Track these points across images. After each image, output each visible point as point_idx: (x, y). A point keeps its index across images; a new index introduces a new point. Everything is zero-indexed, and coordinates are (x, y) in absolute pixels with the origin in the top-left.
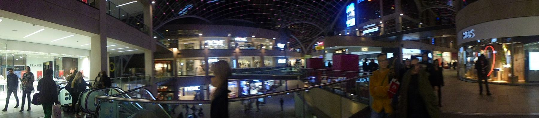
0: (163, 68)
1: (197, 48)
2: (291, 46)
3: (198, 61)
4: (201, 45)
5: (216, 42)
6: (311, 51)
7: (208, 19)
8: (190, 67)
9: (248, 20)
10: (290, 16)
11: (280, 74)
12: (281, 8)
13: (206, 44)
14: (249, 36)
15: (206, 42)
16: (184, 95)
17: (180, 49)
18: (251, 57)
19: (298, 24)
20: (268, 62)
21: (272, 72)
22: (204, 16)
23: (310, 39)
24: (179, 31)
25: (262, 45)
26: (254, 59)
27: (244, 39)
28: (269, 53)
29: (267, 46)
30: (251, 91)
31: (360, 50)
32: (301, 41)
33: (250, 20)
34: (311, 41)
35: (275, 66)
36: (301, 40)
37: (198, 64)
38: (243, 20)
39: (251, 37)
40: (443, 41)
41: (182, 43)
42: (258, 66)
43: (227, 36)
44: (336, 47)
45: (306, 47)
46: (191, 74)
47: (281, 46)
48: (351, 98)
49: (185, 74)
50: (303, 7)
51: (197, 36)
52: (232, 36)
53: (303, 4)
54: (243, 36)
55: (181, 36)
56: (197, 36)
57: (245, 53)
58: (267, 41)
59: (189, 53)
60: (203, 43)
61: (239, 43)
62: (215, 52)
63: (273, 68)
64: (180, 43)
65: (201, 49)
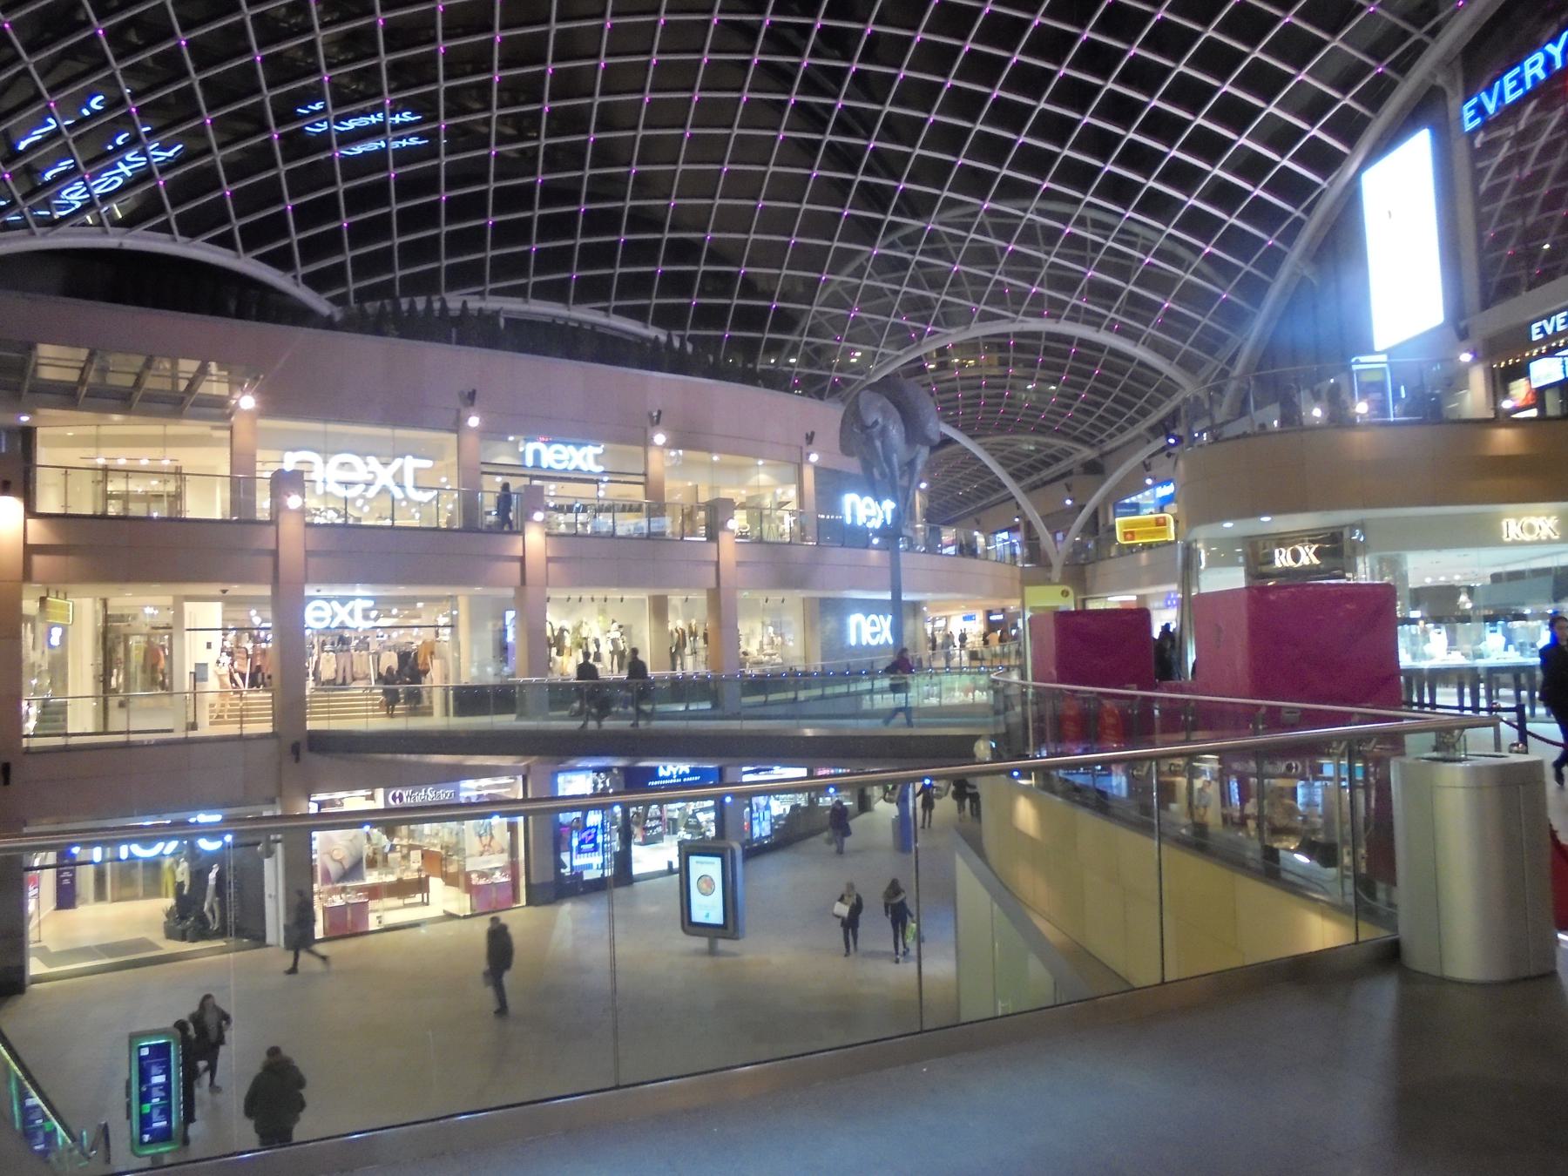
0: (795, 808)
1: (208, 503)
2: (938, 516)
3: (206, 614)
4: (241, 486)
5: (365, 468)
6: (1094, 550)
7: (316, 282)
8: (129, 662)
9: (619, 311)
10: (935, 283)
11: (851, 727)
12: (866, 231)
13: (286, 482)
14: (628, 431)
15: (290, 462)
16: (66, 897)
17: (49, 502)
18: (643, 595)
19: (998, 344)
20: (768, 638)
21: (796, 711)
22: (281, 260)
23: (1088, 453)
24: (46, 351)
25: (727, 506)
26: (660, 609)
27: (585, 457)
28: (781, 565)
29: (757, 512)
30: (637, 851)
31: (1487, 536)
32: (1017, 476)
33: (638, 314)
34: (1095, 469)
35: (816, 664)
36: (1046, 437)
37: (205, 633)
38: (585, 314)
39: (646, 443)
40: (139, 874)
41: (72, 456)
42: (692, 665)
43: (457, 426)
44: (1267, 523)
45: (1057, 520)
46: (148, 720)
47: (865, 510)
48: (1296, 888)
49: (81, 720)
50: (1030, 213)
51: (218, 409)
52: (494, 432)
53: (1028, 191)
54: (579, 435)
55: (67, 396)
56: (218, 409)
57: (597, 560)
58: (763, 478)
59: (121, 546)
60: (265, 472)
61: (551, 488)
62: (361, 551)
63: (799, 679)
64: (43, 455)
65: (242, 521)
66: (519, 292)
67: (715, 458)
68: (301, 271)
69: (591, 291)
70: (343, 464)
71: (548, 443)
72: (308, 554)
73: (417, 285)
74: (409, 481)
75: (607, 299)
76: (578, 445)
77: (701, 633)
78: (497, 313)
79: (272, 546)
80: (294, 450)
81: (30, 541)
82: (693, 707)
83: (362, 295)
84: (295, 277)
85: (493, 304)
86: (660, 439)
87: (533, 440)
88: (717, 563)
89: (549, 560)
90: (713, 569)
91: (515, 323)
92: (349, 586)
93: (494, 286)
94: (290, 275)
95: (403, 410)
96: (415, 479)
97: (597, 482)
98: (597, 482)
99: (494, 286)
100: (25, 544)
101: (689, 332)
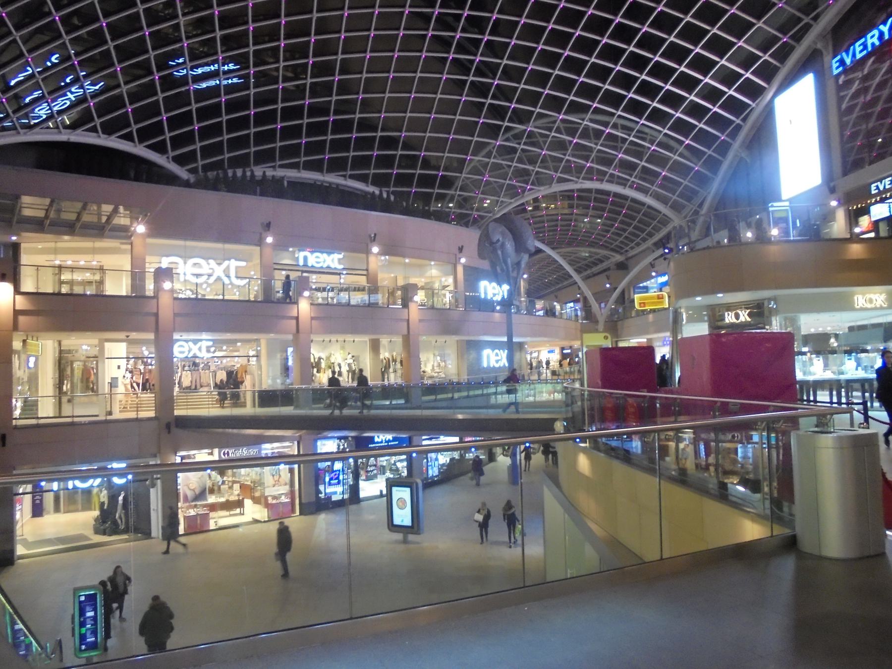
0: (452, 460)
1: (118, 286)
2: (534, 293)
3: (117, 349)
4: (137, 277)
5: (207, 266)
6: (622, 313)
7: (180, 160)
8: (73, 377)
9: (352, 177)
10: (532, 161)
11: (484, 414)
12: (493, 131)
13: (162, 274)
14: (357, 245)
15: (165, 263)
16: (38, 511)
17: (28, 285)
18: (366, 338)
19: (568, 196)
20: (437, 363)
21: (453, 404)
22: (160, 148)
23: (619, 258)
24: (26, 199)
25: (414, 288)
26: (375, 347)
27: (333, 260)
28: (444, 322)
29: (430, 291)
30: (362, 484)
31: (846, 305)
32: (578, 271)
33: (363, 178)
34: (623, 267)
35: (464, 378)
36: (595, 248)
37: (116, 360)
38: (333, 179)
39: (368, 252)
40: (79, 497)
41: (41, 260)
42: (393, 379)
43: (260, 242)
44: (721, 297)
45: (602, 296)
46: (84, 410)
47: (492, 290)
48: (738, 505)
49: (46, 410)
50: (586, 121)
51: (124, 233)
52: (281, 246)
53: (585, 109)
54: (329, 247)
55: (38, 225)
56: (124, 233)
57: (339, 319)
58: (434, 272)
59: (69, 311)
60: (150, 268)
61: (314, 278)
62: (206, 314)
63: (454, 386)
64: (25, 259)
65: (138, 296)
66: (295, 166)
67: (407, 261)
68: (171, 154)
69: (336, 166)
70: (195, 264)
71: (312, 252)
72: (175, 315)
73: (237, 162)
74: (232, 274)
75: (345, 170)
76: (329, 253)
77: (399, 360)
78: (283, 178)
79: (155, 311)
80: (167, 256)
81: (17, 308)
82: (394, 402)
83: (206, 168)
84: (168, 158)
85: (280, 173)
86: (375, 250)
87: (303, 250)
88: (408, 320)
89: (312, 318)
90: (406, 324)
91: (293, 184)
92: (198, 334)
93: (281, 163)
94: (165, 157)
95: (229, 233)
96: (236, 273)
97: (339, 274)
98: (339, 274)
99: (281, 163)
100: (14, 309)
101: (392, 189)
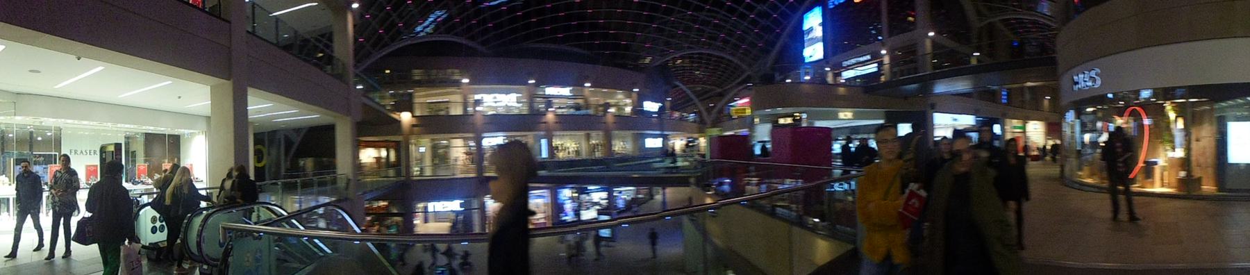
0: (378, 159)
1: (457, 111)
2: (674, 108)
3: (458, 142)
4: (465, 105)
5: (500, 97)
6: (722, 118)
7: (483, 43)
8: (440, 157)
9: (576, 46)
10: (673, 37)
11: (650, 173)
12: (651, 19)
13: (478, 103)
14: (577, 83)
15: (477, 97)
16: (426, 221)
17: (418, 113)
18: (582, 133)
19: (690, 57)
20: (621, 146)
21: (631, 169)
22: (472, 38)
23: (719, 90)
24: (416, 71)
25: (608, 106)
26: (588, 137)
27: (566, 91)
28: (624, 122)
29: (620, 108)
30: (582, 212)
31: (835, 117)
32: (698, 96)
33: (579, 46)
34: (721, 95)
35: (637, 154)
36: (698, 93)
37: (458, 150)
38: (564, 47)
39: (582, 86)
40: (1028, 96)
41: (422, 100)
42: (598, 155)
43: (526, 83)
44: (780, 110)
45: (709, 110)
46: (443, 173)
47: (651, 106)
48: (814, 229)
49: (428, 172)
50: (702, 16)
51: (457, 84)
52: (537, 85)
53: (702, 9)
54: (563, 85)
55: (419, 84)
56: (457, 84)
57: (568, 123)
58: (620, 96)
59: (438, 124)
60: (471, 100)
61: (555, 101)
62: (499, 122)
63: (632, 158)
64: (417, 100)
65: (466, 115)
